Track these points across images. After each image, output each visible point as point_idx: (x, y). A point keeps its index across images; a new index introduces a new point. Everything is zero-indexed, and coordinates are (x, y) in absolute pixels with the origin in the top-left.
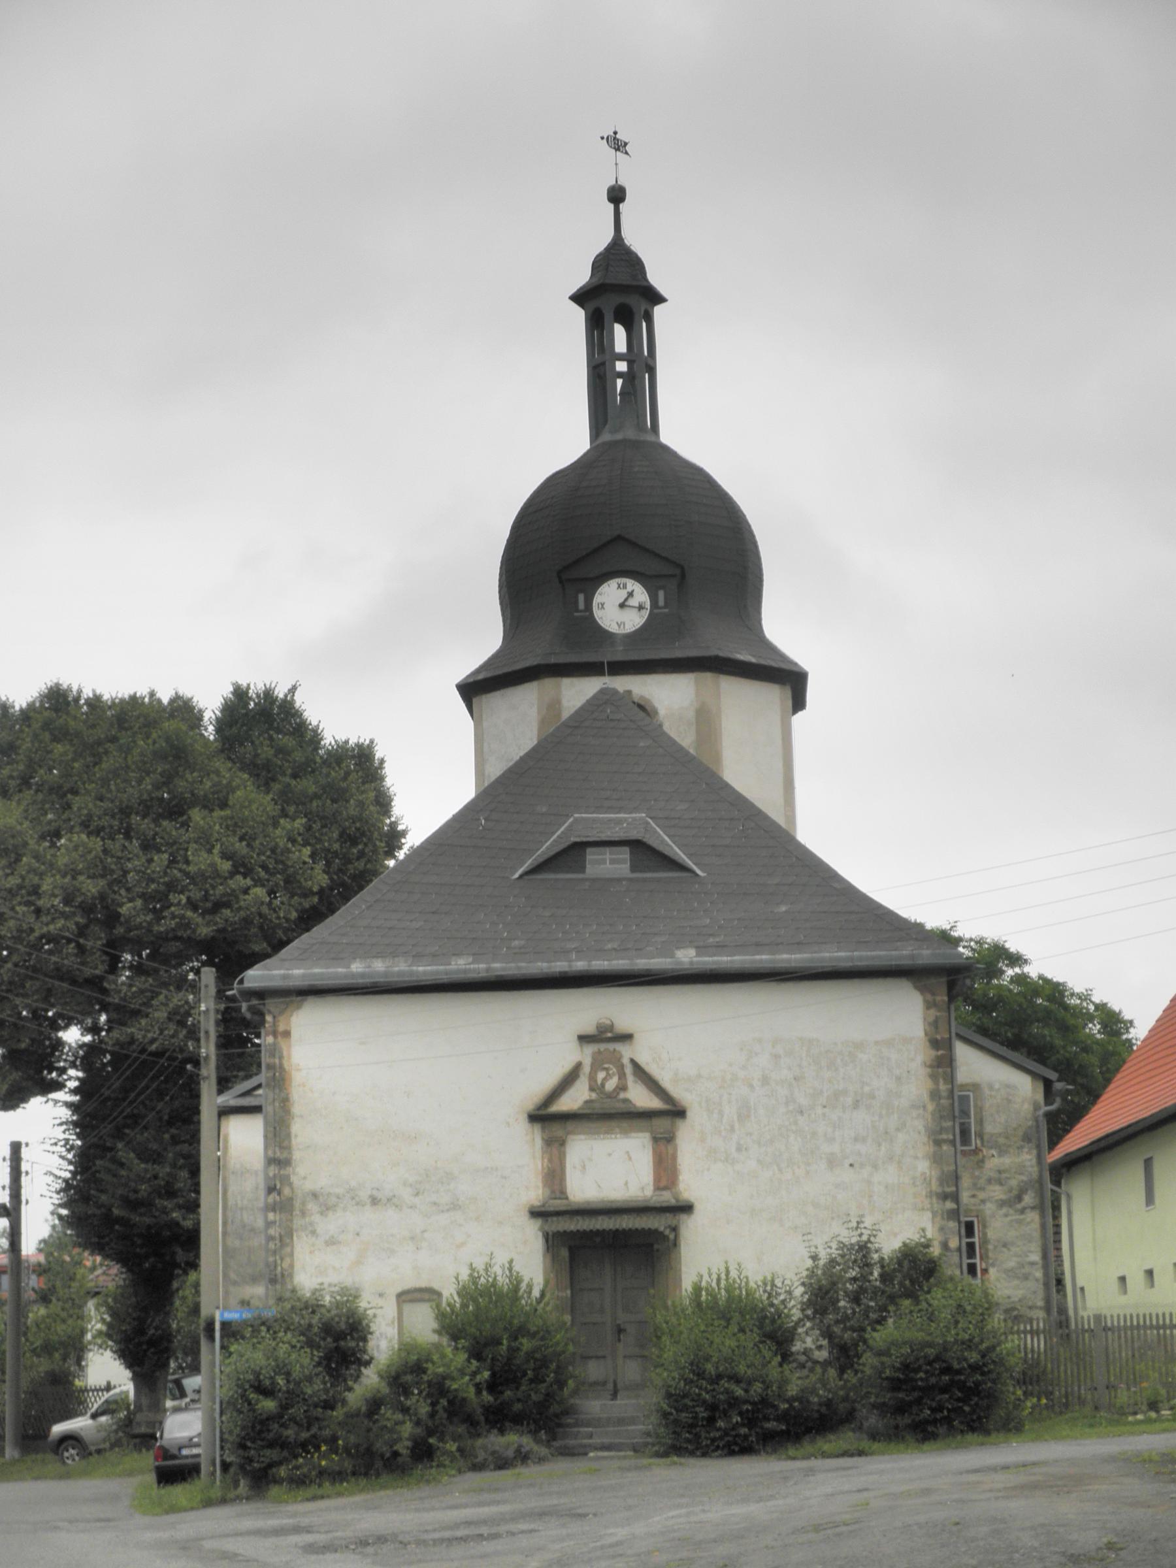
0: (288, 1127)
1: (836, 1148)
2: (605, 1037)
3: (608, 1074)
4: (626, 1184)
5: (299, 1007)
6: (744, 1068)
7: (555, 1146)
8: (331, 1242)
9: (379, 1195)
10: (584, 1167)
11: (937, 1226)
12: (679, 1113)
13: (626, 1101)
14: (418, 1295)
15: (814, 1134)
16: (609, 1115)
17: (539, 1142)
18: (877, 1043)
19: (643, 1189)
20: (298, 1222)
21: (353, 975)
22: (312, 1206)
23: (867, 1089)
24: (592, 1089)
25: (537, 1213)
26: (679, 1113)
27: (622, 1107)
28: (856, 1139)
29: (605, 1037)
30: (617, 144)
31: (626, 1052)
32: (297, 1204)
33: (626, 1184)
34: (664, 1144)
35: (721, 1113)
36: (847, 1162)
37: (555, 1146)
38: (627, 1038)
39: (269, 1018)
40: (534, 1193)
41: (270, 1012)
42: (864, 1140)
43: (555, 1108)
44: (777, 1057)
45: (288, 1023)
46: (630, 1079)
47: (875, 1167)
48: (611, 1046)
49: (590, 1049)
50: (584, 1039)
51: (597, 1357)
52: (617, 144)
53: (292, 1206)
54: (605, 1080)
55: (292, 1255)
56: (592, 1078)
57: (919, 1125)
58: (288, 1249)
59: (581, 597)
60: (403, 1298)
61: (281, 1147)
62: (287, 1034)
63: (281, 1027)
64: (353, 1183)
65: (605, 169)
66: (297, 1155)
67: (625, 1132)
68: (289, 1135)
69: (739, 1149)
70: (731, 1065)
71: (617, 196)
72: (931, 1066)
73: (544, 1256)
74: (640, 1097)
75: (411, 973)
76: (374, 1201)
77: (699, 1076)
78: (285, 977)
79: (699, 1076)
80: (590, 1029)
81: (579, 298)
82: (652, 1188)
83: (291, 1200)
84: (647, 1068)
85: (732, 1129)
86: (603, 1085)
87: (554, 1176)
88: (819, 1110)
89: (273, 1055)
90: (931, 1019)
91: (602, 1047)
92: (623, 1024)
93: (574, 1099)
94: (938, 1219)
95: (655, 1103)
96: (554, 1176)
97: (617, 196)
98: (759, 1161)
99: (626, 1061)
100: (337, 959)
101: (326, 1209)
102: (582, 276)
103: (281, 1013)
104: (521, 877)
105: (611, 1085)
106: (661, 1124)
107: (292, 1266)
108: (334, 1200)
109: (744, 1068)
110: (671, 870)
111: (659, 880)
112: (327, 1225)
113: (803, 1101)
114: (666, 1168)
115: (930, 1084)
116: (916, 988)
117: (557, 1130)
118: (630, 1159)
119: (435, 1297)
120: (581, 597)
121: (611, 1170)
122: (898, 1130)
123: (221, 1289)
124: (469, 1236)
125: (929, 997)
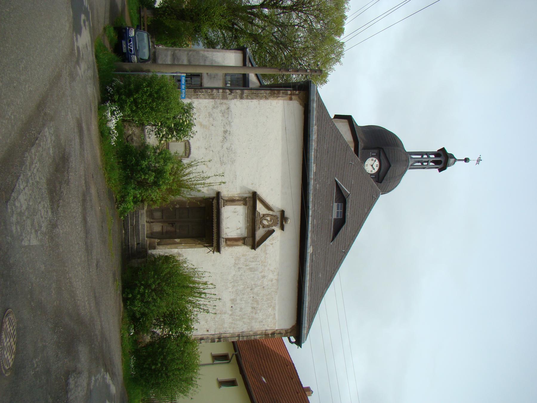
0: (256, 99)
1: (238, 301)
2: (282, 219)
5: (300, 104)
6: (269, 269)
7: (244, 201)
8: (210, 115)
9: (227, 134)
11: (209, 336)
13: (259, 228)
14: (188, 147)
15: (244, 294)
16: (253, 219)
17: (246, 195)
18: (275, 314)
20: (218, 101)
21: (312, 127)
22: (224, 107)
23: (259, 311)
24: (264, 215)
25: (218, 194)
27: (257, 227)
28: (241, 308)
29: (283, 218)
30: (479, 160)
31: (277, 229)
32: (225, 101)
34: (243, 241)
35: (253, 262)
36: (233, 305)
37: (244, 201)
38: (282, 228)
39: (297, 92)
40: (226, 192)
41: (299, 93)
42: (240, 311)
44: (272, 281)
45: (294, 100)
46: (267, 229)
47: (231, 315)
48: (279, 222)
49: (279, 215)
50: (283, 212)
51: (162, 216)
52: (479, 160)
53: (225, 99)
55: (205, 98)
56: (268, 215)
57: (245, 329)
58: (207, 97)
59: (375, 154)
60: (187, 143)
61: (248, 96)
62: (291, 99)
63: (293, 97)
64: (232, 124)
65: (473, 158)
66: (245, 101)
67: (247, 228)
68: (252, 99)
69: (239, 268)
70: (270, 265)
71: (466, 160)
72: (265, 332)
73: (202, 197)
74: (260, 233)
75: (312, 149)
76: (225, 132)
77: (266, 254)
78: (314, 100)
79: (266, 254)
80: (287, 214)
81: (443, 150)
83: (227, 98)
84: (270, 237)
85: (246, 266)
86: (265, 220)
87: (232, 201)
88: (252, 296)
89: (283, 93)
90: (282, 332)
91: (279, 219)
92: (287, 226)
93: (260, 209)
94: (212, 336)
95: (258, 238)
96: (232, 201)
97: (466, 160)
98: (235, 275)
99: (274, 228)
100: (318, 119)
101: (223, 114)
102: (449, 151)
103: (299, 98)
104: (336, 181)
105: (265, 222)
106: (250, 240)
107: (201, 98)
108: (226, 116)
109: (269, 269)
110: (334, 231)
111: (331, 229)
112: (217, 114)
113: (255, 290)
114: (233, 241)
115: (259, 332)
116: (293, 327)
117: (250, 203)
119: (187, 155)
120: (375, 154)
121: (233, 221)
122: (244, 322)
124: (210, 169)
125: (289, 331)
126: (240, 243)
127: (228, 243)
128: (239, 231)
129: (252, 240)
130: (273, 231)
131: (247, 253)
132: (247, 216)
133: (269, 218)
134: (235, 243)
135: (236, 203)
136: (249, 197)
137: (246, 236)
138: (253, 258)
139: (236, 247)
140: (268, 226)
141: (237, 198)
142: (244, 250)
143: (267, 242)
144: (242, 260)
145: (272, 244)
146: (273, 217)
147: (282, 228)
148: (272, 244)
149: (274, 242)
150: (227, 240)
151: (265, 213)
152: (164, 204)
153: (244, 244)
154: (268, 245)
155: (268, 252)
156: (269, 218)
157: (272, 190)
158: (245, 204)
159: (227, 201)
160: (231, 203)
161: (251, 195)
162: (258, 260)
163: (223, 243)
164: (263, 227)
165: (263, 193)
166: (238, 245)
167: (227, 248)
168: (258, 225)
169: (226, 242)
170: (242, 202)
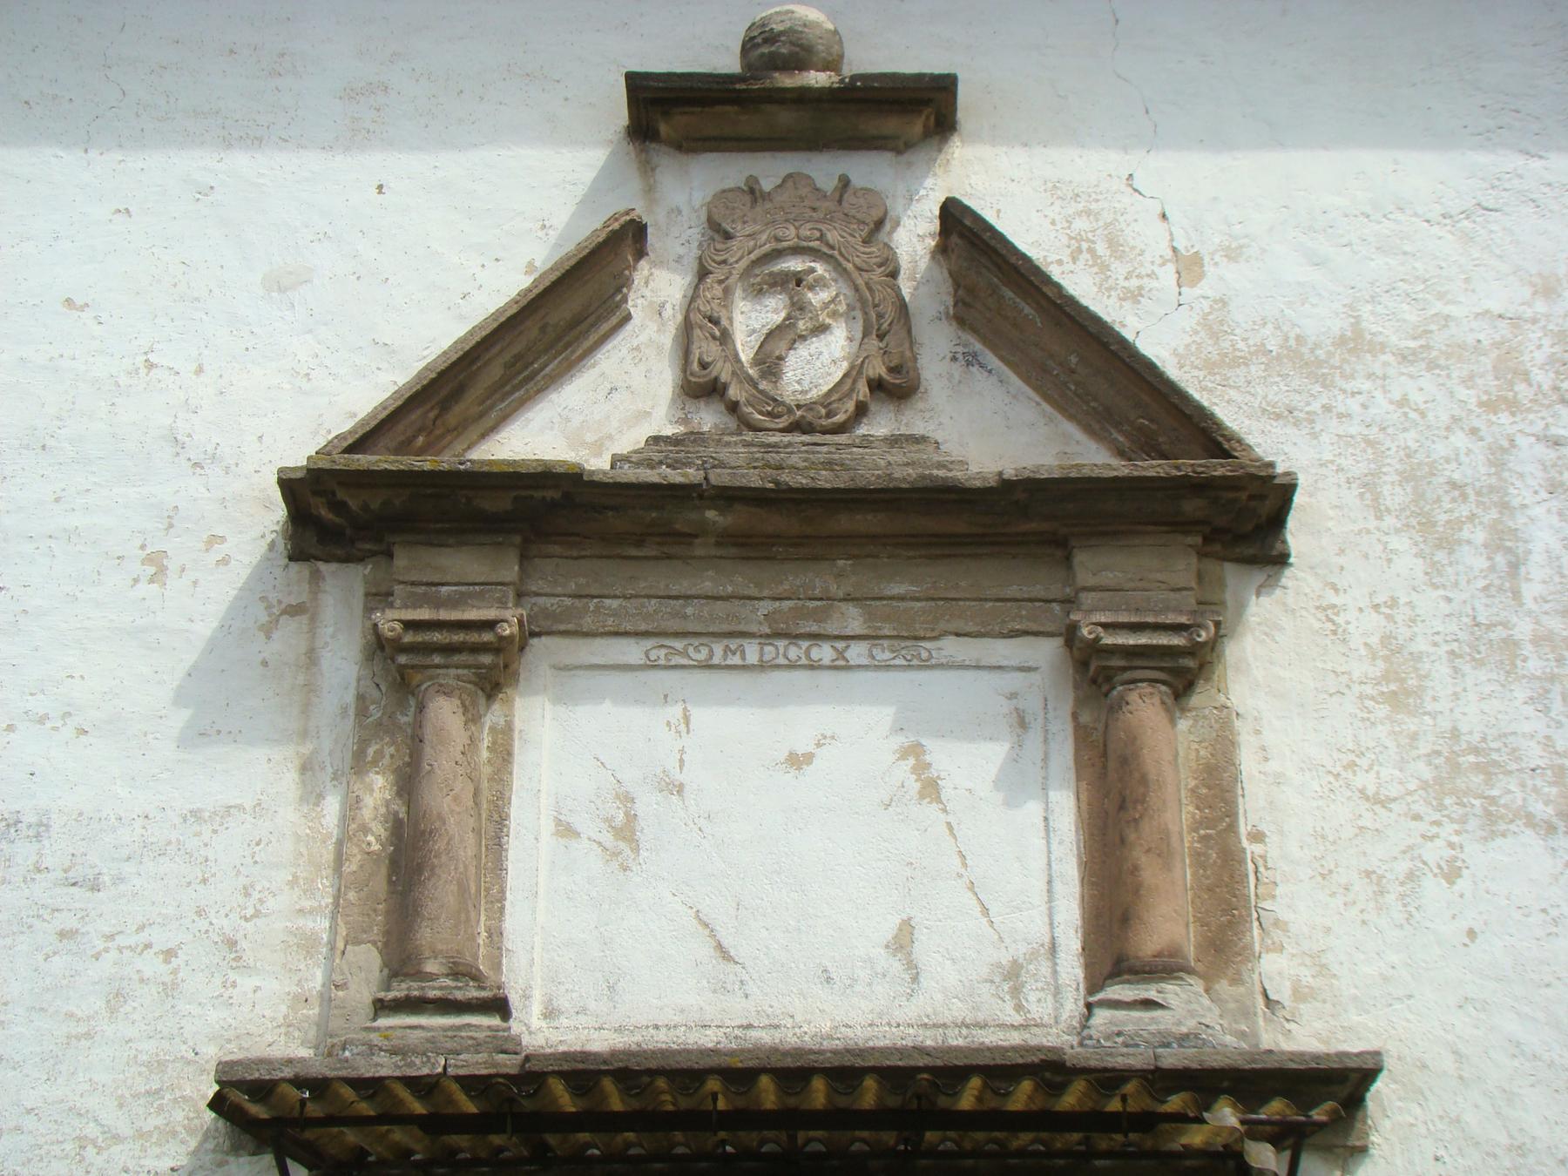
3: (798, 307)
4: (903, 941)
7: (431, 672)
10: (627, 832)
12: (1240, 517)
16: (768, 542)
17: (342, 666)
19: (1013, 974)
24: (701, 387)
26: (1240, 517)
27: (902, 469)
33: (903, 941)
35: (1507, 549)
38: (918, 110)
43: (535, 436)
49: (687, 190)
54: (782, 336)
56: (700, 325)
67: (905, 635)
74: (983, 427)
77: (1355, 342)
79: (1355, 342)
82: (1072, 968)
86: (769, 364)
87: (411, 882)
91: (770, 169)
93: (600, 416)
96: (411, 882)
105: (820, 364)
106: (1122, 587)
114: (1147, 868)
117: (472, 584)
118: (931, 789)
123: (882, 236)
126: (1166, 737)
127: (1169, 922)
128: (973, 764)
129: (1122, 530)
130: (962, 230)
131: (1364, 627)
132: (696, 638)
133: (751, 320)
134: (1176, 813)
135: (447, 800)
136: (379, 597)
137: (1045, 652)
138: (1440, 541)
139: (1253, 808)
140: (885, 320)
141: (378, 789)
142: (1299, 693)
143: (1161, 337)
144: (1478, 705)
145: (1189, 267)
146: (740, 252)
147: (918, 110)
148: (1189, 267)
149: (1151, 240)
150: (1115, 950)
151: (662, 380)
152: (685, 261)
153: (1185, 669)
154: (1214, 327)
155: (1321, 321)
156: (751, 320)
157: (280, 285)
158: (490, 668)
159: (401, 960)
160: (441, 893)
161: (341, 588)
162: (1474, 467)
163: (1189, 1018)
164: (896, 388)
165: (329, 390)
166: (1218, 789)
167: (1275, 968)
168: (880, 448)
169: (1166, 968)
170: (445, 712)
